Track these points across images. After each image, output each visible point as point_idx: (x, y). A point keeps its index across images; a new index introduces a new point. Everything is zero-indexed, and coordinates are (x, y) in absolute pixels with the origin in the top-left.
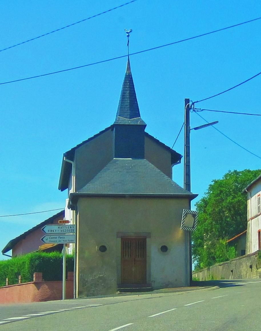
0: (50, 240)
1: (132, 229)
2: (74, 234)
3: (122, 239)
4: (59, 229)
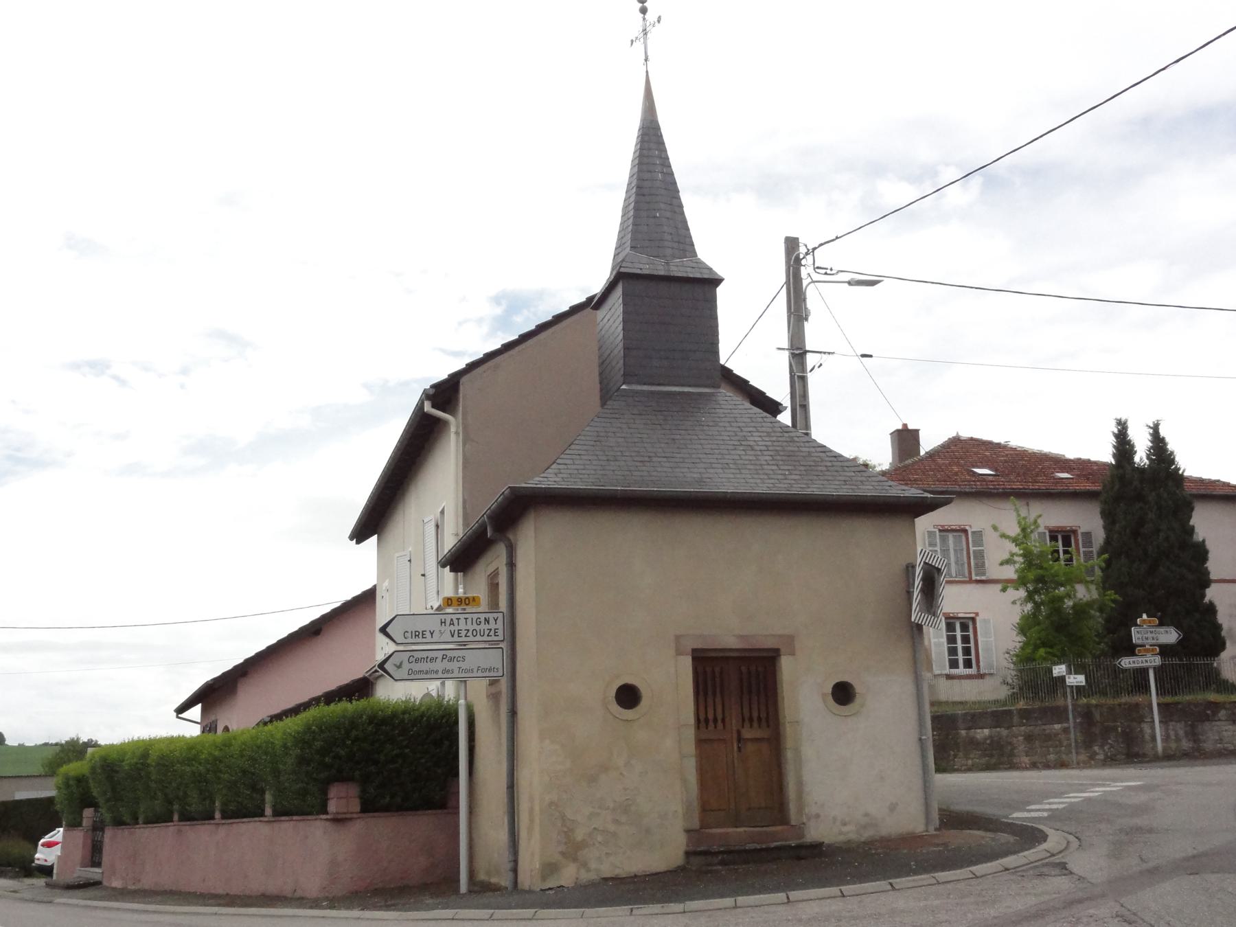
0: (411, 666)
1: (729, 631)
2: (717, 670)
3: (693, 659)
4: (443, 628)
